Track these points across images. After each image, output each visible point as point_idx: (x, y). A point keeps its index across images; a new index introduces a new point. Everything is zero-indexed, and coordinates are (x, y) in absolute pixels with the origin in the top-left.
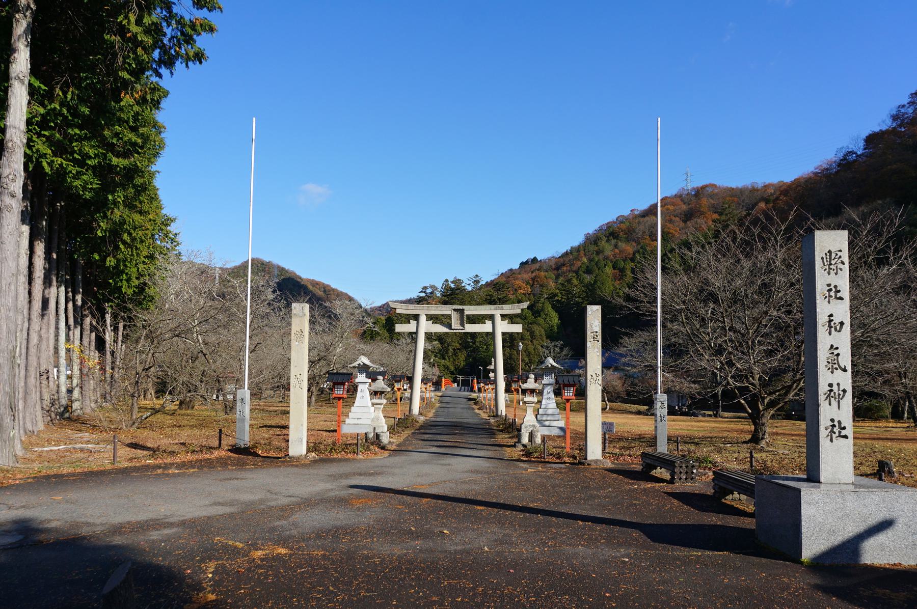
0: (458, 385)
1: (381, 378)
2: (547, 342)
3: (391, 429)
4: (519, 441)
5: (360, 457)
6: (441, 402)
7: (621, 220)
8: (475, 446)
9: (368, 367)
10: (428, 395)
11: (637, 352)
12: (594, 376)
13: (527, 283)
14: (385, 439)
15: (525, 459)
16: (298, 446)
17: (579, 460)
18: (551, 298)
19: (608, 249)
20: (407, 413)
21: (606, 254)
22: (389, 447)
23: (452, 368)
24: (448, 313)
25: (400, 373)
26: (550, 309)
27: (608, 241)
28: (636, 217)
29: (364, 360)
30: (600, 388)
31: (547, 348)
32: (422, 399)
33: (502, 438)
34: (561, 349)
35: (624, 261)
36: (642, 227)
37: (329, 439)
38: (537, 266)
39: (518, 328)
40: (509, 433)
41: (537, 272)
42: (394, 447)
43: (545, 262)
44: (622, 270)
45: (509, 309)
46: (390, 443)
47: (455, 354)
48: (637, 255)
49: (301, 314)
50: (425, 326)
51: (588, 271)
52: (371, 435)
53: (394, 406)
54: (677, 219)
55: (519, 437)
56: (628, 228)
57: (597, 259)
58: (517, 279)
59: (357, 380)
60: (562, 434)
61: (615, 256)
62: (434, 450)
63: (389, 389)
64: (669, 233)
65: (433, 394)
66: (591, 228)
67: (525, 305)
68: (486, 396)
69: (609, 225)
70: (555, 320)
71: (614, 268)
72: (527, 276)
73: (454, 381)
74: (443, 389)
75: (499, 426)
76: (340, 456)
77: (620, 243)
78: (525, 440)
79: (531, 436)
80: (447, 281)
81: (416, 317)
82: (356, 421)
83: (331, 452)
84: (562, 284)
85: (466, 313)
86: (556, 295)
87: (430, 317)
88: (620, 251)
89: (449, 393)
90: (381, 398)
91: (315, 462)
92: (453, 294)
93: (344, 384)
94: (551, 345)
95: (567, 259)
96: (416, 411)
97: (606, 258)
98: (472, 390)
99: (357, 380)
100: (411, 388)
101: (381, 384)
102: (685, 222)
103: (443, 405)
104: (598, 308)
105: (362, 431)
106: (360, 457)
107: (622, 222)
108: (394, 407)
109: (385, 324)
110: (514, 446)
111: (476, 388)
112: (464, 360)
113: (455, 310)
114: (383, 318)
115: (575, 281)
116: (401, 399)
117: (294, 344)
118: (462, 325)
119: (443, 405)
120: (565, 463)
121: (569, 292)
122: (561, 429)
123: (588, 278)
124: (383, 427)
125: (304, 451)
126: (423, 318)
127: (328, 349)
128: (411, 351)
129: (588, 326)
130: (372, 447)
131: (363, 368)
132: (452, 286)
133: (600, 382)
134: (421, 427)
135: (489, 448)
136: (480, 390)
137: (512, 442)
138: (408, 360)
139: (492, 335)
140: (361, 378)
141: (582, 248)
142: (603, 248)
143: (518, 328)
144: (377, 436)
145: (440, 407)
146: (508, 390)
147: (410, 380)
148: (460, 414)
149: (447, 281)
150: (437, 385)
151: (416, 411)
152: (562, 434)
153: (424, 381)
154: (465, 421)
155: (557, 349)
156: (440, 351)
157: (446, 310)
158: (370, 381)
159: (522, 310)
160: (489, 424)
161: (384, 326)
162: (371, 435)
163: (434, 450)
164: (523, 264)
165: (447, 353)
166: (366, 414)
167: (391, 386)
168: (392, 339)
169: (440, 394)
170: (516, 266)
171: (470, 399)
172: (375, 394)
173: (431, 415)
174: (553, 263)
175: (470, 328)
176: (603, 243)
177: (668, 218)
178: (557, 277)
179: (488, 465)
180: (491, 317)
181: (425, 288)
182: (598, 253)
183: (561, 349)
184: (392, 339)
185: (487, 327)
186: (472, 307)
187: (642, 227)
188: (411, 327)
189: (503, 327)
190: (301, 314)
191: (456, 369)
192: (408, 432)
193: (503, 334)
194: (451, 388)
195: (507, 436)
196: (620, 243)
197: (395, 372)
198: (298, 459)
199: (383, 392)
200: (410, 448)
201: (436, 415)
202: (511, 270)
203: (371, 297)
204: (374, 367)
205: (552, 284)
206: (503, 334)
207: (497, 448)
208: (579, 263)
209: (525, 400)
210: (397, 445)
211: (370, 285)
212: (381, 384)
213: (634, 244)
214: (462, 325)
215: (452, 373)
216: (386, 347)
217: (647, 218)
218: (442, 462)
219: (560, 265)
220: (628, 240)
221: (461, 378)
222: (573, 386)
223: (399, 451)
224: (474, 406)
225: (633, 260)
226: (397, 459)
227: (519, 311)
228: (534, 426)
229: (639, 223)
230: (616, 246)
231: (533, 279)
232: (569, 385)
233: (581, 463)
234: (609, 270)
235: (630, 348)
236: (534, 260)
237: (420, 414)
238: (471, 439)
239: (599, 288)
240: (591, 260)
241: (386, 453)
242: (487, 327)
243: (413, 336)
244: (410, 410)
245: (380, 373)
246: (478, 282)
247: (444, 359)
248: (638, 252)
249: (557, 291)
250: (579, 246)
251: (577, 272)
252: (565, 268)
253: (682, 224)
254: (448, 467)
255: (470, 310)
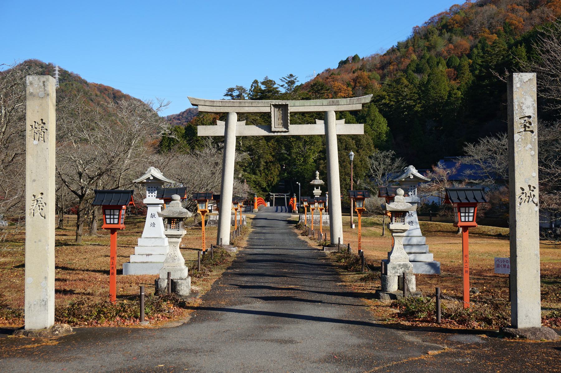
0: (271, 205)
1: (177, 197)
2: (375, 152)
3: (195, 270)
4: (384, 288)
5: (145, 324)
6: (254, 226)
7: (455, 10)
8: (324, 297)
9: (160, 182)
10: (238, 218)
11: (485, 162)
12: (527, 189)
13: (348, 85)
14: (185, 289)
15: (407, 323)
16: (40, 312)
17: (503, 329)
18: (377, 101)
19: (441, 44)
20: (215, 243)
21: (438, 50)
22: (191, 302)
23: (265, 185)
24: (267, 110)
25: (203, 191)
26: (377, 113)
27: (441, 35)
28: (472, 6)
29: (155, 173)
30: (537, 209)
31: (376, 159)
32: (233, 223)
33: (351, 280)
34: (393, 160)
35: (460, 57)
36: (479, 18)
37: (99, 287)
38: (359, 65)
39: (358, 129)
40: (358, 272)
41: (359, 72)
42: (198, 302)
43: (368, 61)
44: (458, 69)
45: (347, 105)
46: (193, 293)
47: (267, 167)
48: (475, 50)
49: (41, 94)
50: (237, 129)
51: (419, 70)
52: (164, 284)
53: (196, 232)
54: (521, 8)
55: (384, 280)
56: (464, 20)
57: (428, 56)
58: (337, 80)
59: (145, 201)
60: (432, 272)
61: (449, 52)
62: (260, 306)
63: (190, 214)
64: (511, 24)
65: (244, 216)
66: (421, 18)
67: (367, 99)
68: (316, 216)
69: (441, 17)
70: (384, 127)
71: (448, 65)
72: (348, 77)
73: (267, 200)
74: (256, 210)
75: (339, 260)
76: (112, 324)
77: (454, 37)
78: (393, 287)
79: (402, 281)
80: (256, 82)
81: (224, 117)
82: (145, 259)
83: (98, 317)
84: (390, 85)
85: (291, 109)
86: (383, 98)
87: (241, 116)
88: (455, 47)
89: (263, 214)
90: (178, 228)
91: (66, 340)
92: (265, 92)
93: (120, 208)
94: (381, 155)
95: (393, 57)
96: (226, 239)
97: (439, 55)
98: (291, 210)
99: (145, 201)
100: (219, 209)
101: (177, 206)
102: (530, 11)
103: (258, 230)
104: (531, 77)
105: (152, 272)
106: (145, 324)
107: (456, 13)
108: (197, 234)
109: (186, 134)
110: (376, 296)
111: (296, 209)
112: (284, 172)
113: (275, 106)
114: (183, 127)
115: (405, 82)
116: (206, 222)
117: (31, 143)
118: (286, 126)
119: (258, 230)
120: (474, 332)
121: (398, 93)
122: (431, 265)
123: (418, 78)
124: (181, 271)
125: (50, 320)
126: (233, 118)
127: (111, 162)
128: (217, 164)
129: (516, 107)
130: (164, 305)
131: (154, 184)
132: (263, 87)
133: (537, 200)
134: (236, 264)
135: (340, 299)
136: (302, 211)
137: (371, 287)
138: (213, 174)
139: (325, 138)
140: (151, 198)
141: (410, 44)
142: (436, 43)
143: (358, 129)
144: (173, 285)
145: (253, 232)
146: (346, 210)
147: (218, 199)
148: (281, 242)
149: (256, 82)
150: (249, 205)
151: (226, 239)
152: (432, 272)
153: (236, 200)
154: (293, 252)
155: (388, 161)
156: (250, 164)
157: (263, 107)
158: (162, 201)
159: (363, 105)
160: (324, 256)
161: (184, 136)
162: (164, 284)
163: (260, 306)
164: (342, 63)
165: (258, 167)
166: (158, 250)
167: (192, 208)
168: (193, 148)
169: (253, 216)
170: (334, 66)
171: (290, 222)
172: (170, 221)
173: (244, 244)
174: (377, 62)
175: (296, 130)
176: (435, 37)
177: (510, 7)
178: (383, 77)
179: (355, 341)
180: (323, 116)
181: (231, 90)
182: (429, 49)
183: (393, 160)
184: (193, 148)
185: (318, 128)
186: (298, 102)
187: (479, 18)
188: (218, 130)
189: (338, 128)
190: (41, 94)
191: (268, 186)
192: (216, 274)
193: (340, 137)
194: (264, 208)
195: (357, 276)
196: (454, 37)
197: (197, 189)
198: (37, 336)
199: (181, 219)
200: (223, 304)
201: (251, 245)
202: (328, 71)
203: (170, 104)
204: (170, 182)
205: (377, 86)
206: (340, 137)
207: (350, 300)
208: (407, 62)
209: (392, 227)
210: (204, 298)
211: (166, 90)
212: (177, 206)
213: (471, 38)
214: (286, 126)
215: (264, 190)
216: (185, 159)
217: (486, 8)
218: (277, 334)
219: (385, 64)
220: (463, 34)
221: (274, 196)
222: (474, 205)
223: (205, 310)
224: (296, 231)
225: (469, 56)
226: (206, 329)
227: (359, 107)
228: (405, 266)
229: (476, 13)
230: (450, 40)
231: (355, 80)
232: (469, 205)
233: (503, 334)
234: (442, 68)
235: (476, 157)
236: (355, 58)
237: (232, 244)
238: (308, 283)
239: (433, 88)
240: (421, 57)
241: (187, 315)
242: (318, 128)
243: (220, 142)
244: (219, 238)
245: (177, 191)
246: (292, 82)
247: (255, 174)
248: (476, 46)
249: (385, 93)
250: (407, 42)
251: (405, 71)
252: (391, 67)
253: (526, 14)
254: (290, 348)
255: (296, 106)
